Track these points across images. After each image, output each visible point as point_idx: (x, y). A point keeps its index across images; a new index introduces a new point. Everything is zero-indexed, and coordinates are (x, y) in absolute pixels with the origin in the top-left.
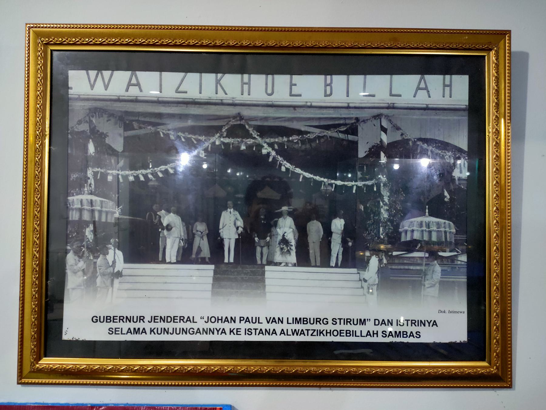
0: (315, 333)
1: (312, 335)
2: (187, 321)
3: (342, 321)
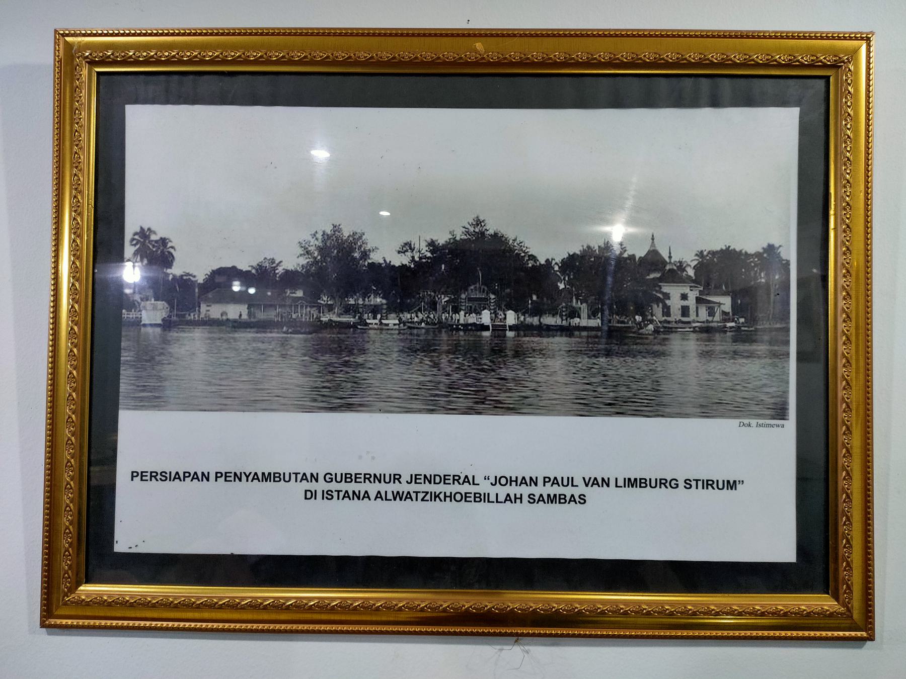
0: (428, 497)
1: (423, 500)
2: (464, 481)
3: (700, 483)
